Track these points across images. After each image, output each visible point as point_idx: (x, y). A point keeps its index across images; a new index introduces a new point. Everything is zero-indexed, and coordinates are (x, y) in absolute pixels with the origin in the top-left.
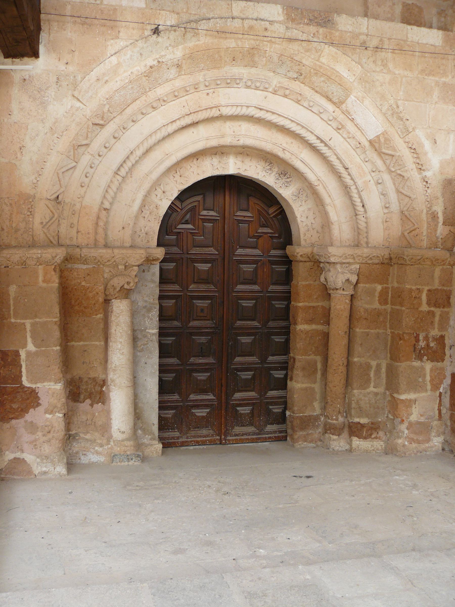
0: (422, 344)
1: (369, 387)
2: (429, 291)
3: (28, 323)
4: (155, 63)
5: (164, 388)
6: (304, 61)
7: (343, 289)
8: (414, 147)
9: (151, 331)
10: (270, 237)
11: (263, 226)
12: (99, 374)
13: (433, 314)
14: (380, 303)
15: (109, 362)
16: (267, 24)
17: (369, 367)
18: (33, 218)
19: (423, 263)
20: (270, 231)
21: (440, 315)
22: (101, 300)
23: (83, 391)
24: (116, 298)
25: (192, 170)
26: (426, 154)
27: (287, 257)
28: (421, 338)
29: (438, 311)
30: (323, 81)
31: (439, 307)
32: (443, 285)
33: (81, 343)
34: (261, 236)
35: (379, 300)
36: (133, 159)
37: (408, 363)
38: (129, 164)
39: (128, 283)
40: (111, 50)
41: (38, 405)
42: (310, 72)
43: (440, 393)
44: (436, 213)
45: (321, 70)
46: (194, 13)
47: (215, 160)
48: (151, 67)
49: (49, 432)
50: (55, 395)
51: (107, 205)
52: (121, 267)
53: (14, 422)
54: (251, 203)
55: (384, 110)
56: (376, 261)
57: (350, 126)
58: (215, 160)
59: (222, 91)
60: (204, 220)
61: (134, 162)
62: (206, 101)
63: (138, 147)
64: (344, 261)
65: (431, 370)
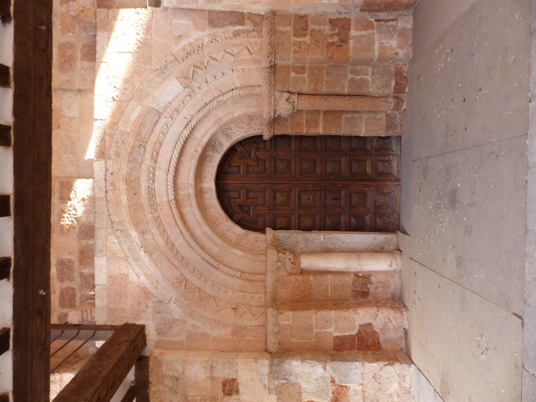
0: (336, 39)
1: (367, 79)
2: (294, 36)
3: (315, 331)
4: (142, 249)
5: (360, 228)
6: (131, 144)
7: (294, 102)
8: (186, 55)
9: (322, 239)
10: (257, 150)
11: (250, 155)
12: (349, 279)
13: (313, 30)
14: (305, 73)
15: (343, 270)
16: (109, 173)
17: (352, 80)
18: (248, 326)
19: (273, 43)
20: (253, 150)
21: (314, 24)
22: (300, 278)
23: (362, 292)
24: (300, 266)
25: (213, 213)
26: (190, 44)
27: (271, 139)
28: (331, 40)
29: (311, 26)
30: (144, 128)
31: (307, 26)
32: (290, 23)
33: (329, 290)
34: (257, 157)
35: (302, 74)
36: (207, 258)
37: (351, 51)
38: (211, 260)
39: (290, 259)
40: (136, 279)
41: (370, 324)
42: (138, 139)
43: (376, 20)
44: (235, 33)
45: (136, 131)
46: (106, 224)
47: (207, 196)
48: (145, 252)
49: (389, 318)
50: (365, 314)
51: (238, 274)
52: (279, 264)
53: (380, 341)
54: (235, 164)
55: (160, 80)
56: (273, 78)
57: (174, 105)
58: (205, 197)
59: (158, 200)
60: (247, 198)
61: (209, 257)
62: (167, 211)
63: (199, 255)
64: (273, 104)
65: (357, 30)
